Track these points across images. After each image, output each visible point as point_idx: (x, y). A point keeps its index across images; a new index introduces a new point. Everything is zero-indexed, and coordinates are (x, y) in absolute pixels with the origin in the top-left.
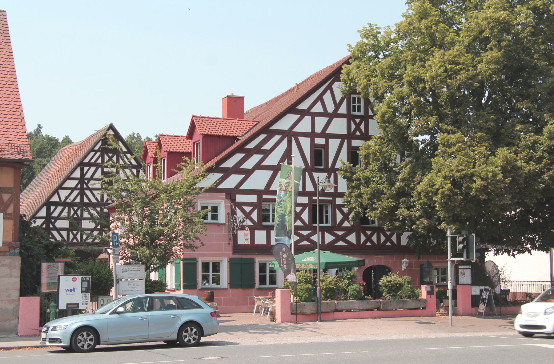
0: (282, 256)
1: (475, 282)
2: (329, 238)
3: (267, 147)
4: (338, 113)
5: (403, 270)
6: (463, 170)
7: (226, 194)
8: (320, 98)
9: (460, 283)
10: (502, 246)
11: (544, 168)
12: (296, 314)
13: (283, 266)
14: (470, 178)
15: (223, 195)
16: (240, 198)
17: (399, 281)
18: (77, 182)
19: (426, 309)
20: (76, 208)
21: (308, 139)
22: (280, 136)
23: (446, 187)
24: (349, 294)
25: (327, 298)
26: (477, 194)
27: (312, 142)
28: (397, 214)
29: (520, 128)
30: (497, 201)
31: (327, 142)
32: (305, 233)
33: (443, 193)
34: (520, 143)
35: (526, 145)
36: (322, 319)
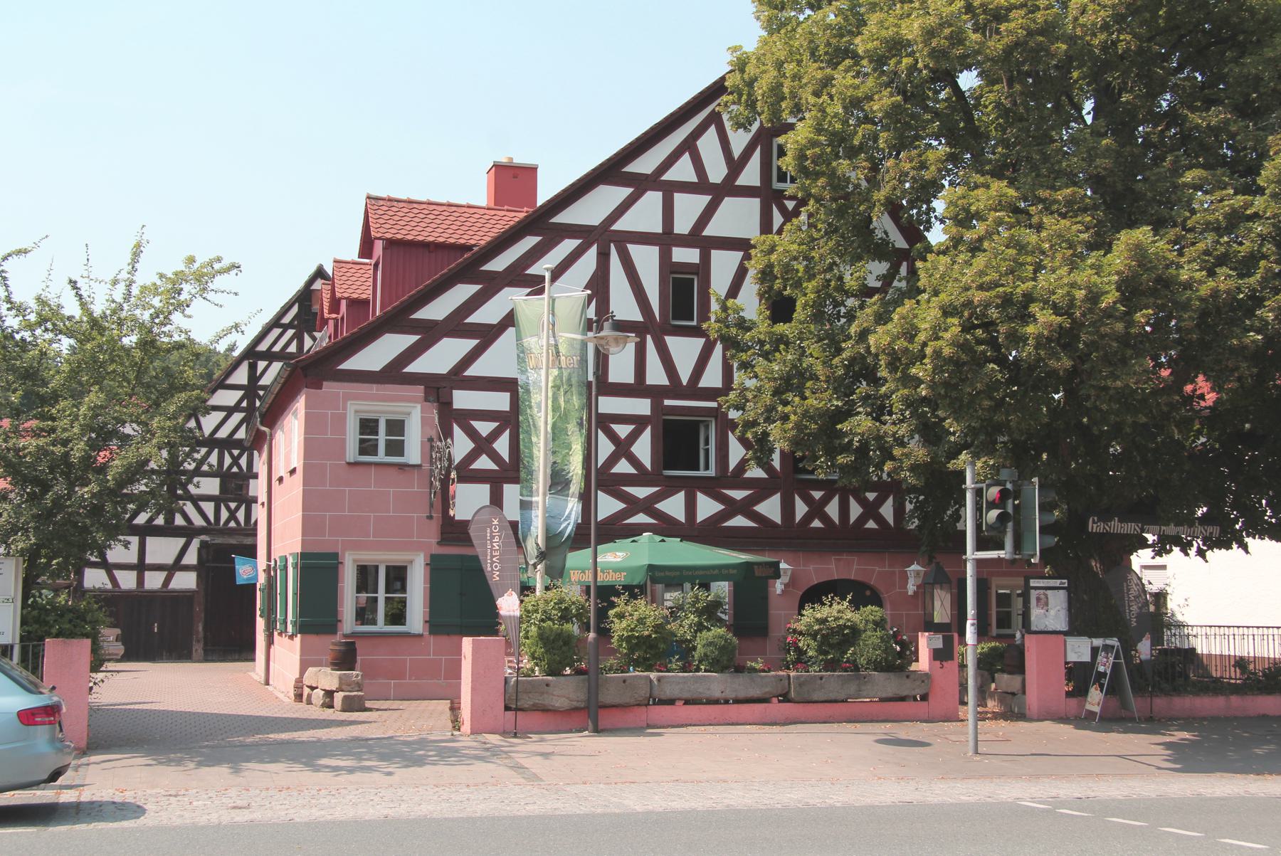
0: (492, 543)
1: (1079, 624)
2: (707, 507)
3: (543, 267)
4: (736, 184)
5: (910, 593)
6: (997, 286)
7: (426, 388)
8: (689, 146)
9: (1034, 628)
10: (1163, 528)
11: (1263, 288)
12: (517, 709)
13: (493, 570)
14: (1019, 309)
15: (419, 391)
16: (463, 399)
17: (849, 620)
18: (240, 393)
19: (930, 698)
20: (236, 452)
21: (655, 250)
22: (578, 242)
23: (947, 335)
24: (696, 655)
25: (630, 662)
26: (1039, 354)
27: (665, 257)
28: (841, 430)
29: (1193, 179)
30: (1106, 378)
31: (706, 259)
32: (641, 492)
33: (937, 354)
34: (1189, 218)
35: (1208, 223)
36: (600, 727)
